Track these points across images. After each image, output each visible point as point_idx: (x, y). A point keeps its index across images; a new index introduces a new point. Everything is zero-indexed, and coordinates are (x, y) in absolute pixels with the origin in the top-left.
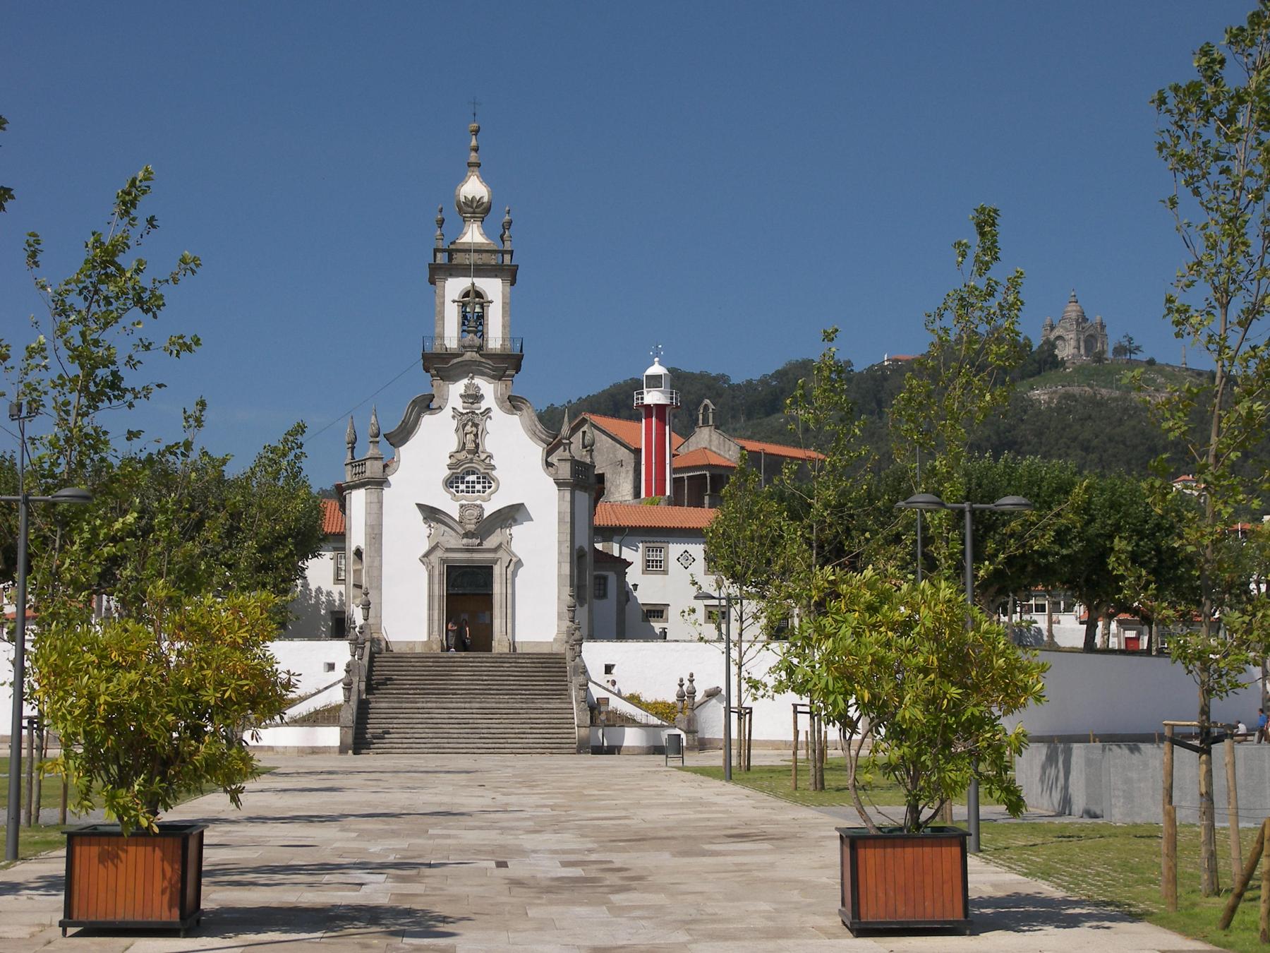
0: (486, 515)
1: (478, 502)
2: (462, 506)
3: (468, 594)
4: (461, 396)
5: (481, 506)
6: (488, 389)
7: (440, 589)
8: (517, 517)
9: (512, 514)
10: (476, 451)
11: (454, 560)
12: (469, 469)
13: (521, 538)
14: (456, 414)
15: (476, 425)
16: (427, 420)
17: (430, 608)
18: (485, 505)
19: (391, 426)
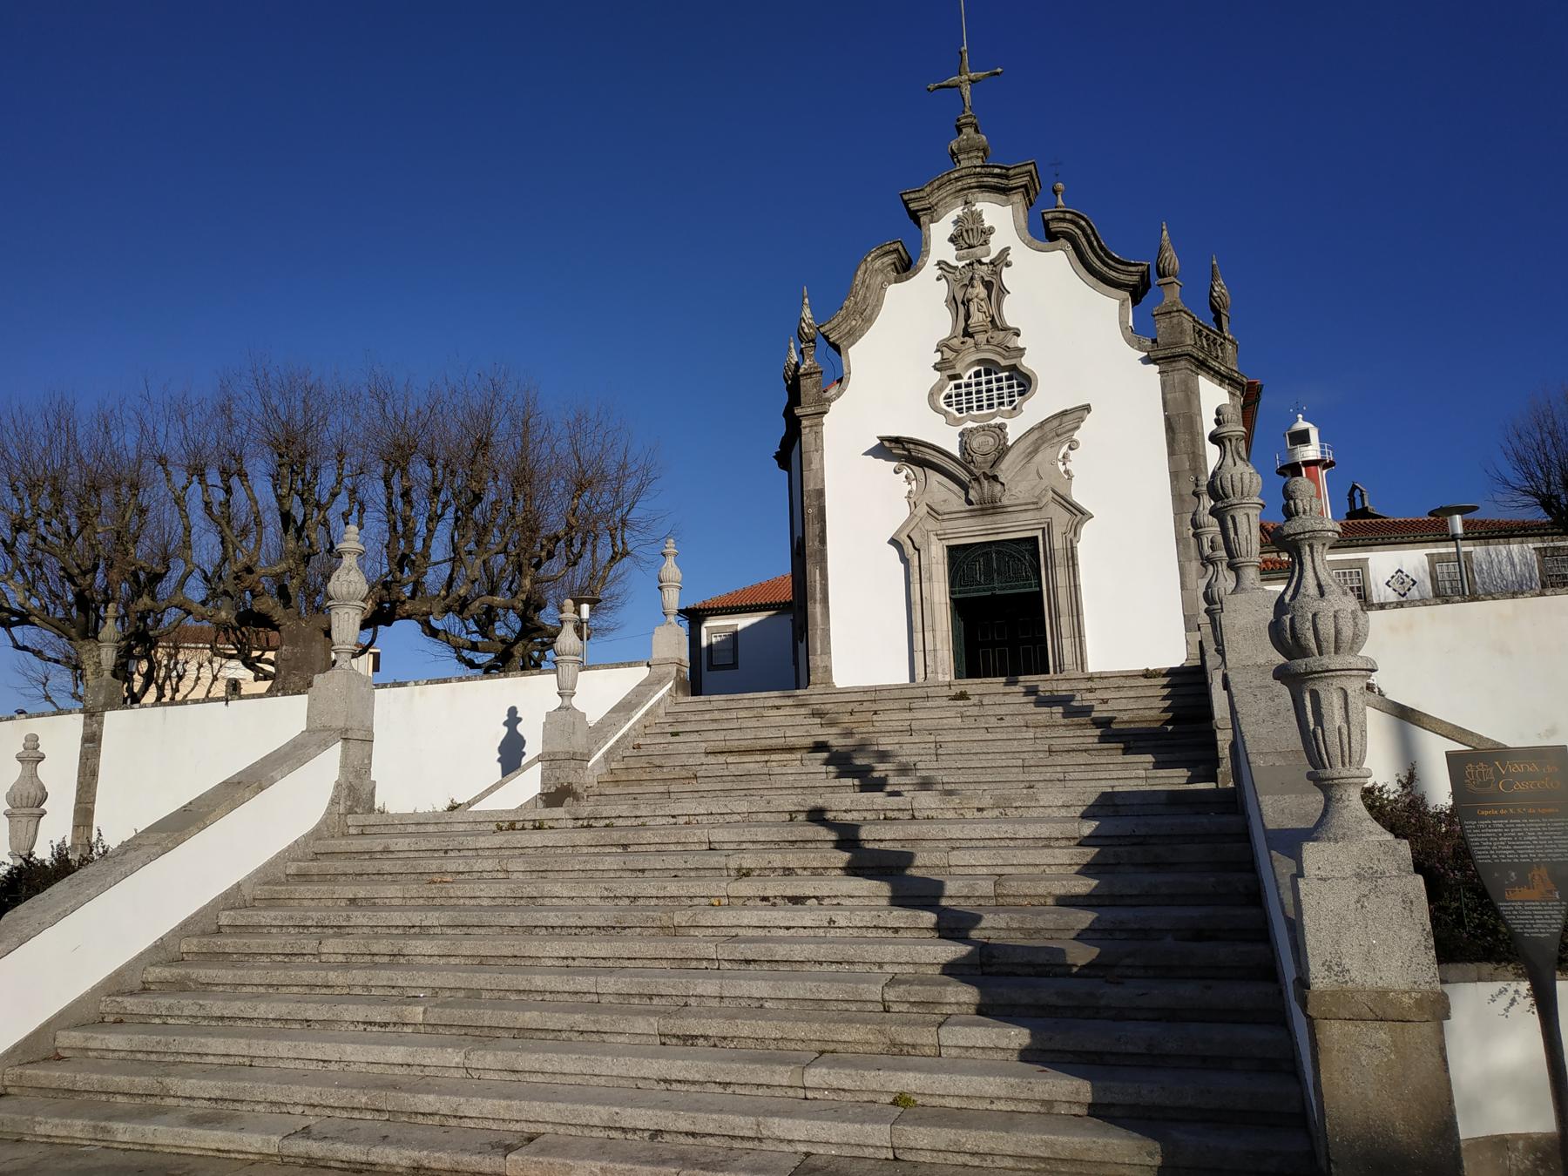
1: (998, 420)
4: (952, 240)
6: (1001, 218)
9: (1064, 424)
12: (986, 362)
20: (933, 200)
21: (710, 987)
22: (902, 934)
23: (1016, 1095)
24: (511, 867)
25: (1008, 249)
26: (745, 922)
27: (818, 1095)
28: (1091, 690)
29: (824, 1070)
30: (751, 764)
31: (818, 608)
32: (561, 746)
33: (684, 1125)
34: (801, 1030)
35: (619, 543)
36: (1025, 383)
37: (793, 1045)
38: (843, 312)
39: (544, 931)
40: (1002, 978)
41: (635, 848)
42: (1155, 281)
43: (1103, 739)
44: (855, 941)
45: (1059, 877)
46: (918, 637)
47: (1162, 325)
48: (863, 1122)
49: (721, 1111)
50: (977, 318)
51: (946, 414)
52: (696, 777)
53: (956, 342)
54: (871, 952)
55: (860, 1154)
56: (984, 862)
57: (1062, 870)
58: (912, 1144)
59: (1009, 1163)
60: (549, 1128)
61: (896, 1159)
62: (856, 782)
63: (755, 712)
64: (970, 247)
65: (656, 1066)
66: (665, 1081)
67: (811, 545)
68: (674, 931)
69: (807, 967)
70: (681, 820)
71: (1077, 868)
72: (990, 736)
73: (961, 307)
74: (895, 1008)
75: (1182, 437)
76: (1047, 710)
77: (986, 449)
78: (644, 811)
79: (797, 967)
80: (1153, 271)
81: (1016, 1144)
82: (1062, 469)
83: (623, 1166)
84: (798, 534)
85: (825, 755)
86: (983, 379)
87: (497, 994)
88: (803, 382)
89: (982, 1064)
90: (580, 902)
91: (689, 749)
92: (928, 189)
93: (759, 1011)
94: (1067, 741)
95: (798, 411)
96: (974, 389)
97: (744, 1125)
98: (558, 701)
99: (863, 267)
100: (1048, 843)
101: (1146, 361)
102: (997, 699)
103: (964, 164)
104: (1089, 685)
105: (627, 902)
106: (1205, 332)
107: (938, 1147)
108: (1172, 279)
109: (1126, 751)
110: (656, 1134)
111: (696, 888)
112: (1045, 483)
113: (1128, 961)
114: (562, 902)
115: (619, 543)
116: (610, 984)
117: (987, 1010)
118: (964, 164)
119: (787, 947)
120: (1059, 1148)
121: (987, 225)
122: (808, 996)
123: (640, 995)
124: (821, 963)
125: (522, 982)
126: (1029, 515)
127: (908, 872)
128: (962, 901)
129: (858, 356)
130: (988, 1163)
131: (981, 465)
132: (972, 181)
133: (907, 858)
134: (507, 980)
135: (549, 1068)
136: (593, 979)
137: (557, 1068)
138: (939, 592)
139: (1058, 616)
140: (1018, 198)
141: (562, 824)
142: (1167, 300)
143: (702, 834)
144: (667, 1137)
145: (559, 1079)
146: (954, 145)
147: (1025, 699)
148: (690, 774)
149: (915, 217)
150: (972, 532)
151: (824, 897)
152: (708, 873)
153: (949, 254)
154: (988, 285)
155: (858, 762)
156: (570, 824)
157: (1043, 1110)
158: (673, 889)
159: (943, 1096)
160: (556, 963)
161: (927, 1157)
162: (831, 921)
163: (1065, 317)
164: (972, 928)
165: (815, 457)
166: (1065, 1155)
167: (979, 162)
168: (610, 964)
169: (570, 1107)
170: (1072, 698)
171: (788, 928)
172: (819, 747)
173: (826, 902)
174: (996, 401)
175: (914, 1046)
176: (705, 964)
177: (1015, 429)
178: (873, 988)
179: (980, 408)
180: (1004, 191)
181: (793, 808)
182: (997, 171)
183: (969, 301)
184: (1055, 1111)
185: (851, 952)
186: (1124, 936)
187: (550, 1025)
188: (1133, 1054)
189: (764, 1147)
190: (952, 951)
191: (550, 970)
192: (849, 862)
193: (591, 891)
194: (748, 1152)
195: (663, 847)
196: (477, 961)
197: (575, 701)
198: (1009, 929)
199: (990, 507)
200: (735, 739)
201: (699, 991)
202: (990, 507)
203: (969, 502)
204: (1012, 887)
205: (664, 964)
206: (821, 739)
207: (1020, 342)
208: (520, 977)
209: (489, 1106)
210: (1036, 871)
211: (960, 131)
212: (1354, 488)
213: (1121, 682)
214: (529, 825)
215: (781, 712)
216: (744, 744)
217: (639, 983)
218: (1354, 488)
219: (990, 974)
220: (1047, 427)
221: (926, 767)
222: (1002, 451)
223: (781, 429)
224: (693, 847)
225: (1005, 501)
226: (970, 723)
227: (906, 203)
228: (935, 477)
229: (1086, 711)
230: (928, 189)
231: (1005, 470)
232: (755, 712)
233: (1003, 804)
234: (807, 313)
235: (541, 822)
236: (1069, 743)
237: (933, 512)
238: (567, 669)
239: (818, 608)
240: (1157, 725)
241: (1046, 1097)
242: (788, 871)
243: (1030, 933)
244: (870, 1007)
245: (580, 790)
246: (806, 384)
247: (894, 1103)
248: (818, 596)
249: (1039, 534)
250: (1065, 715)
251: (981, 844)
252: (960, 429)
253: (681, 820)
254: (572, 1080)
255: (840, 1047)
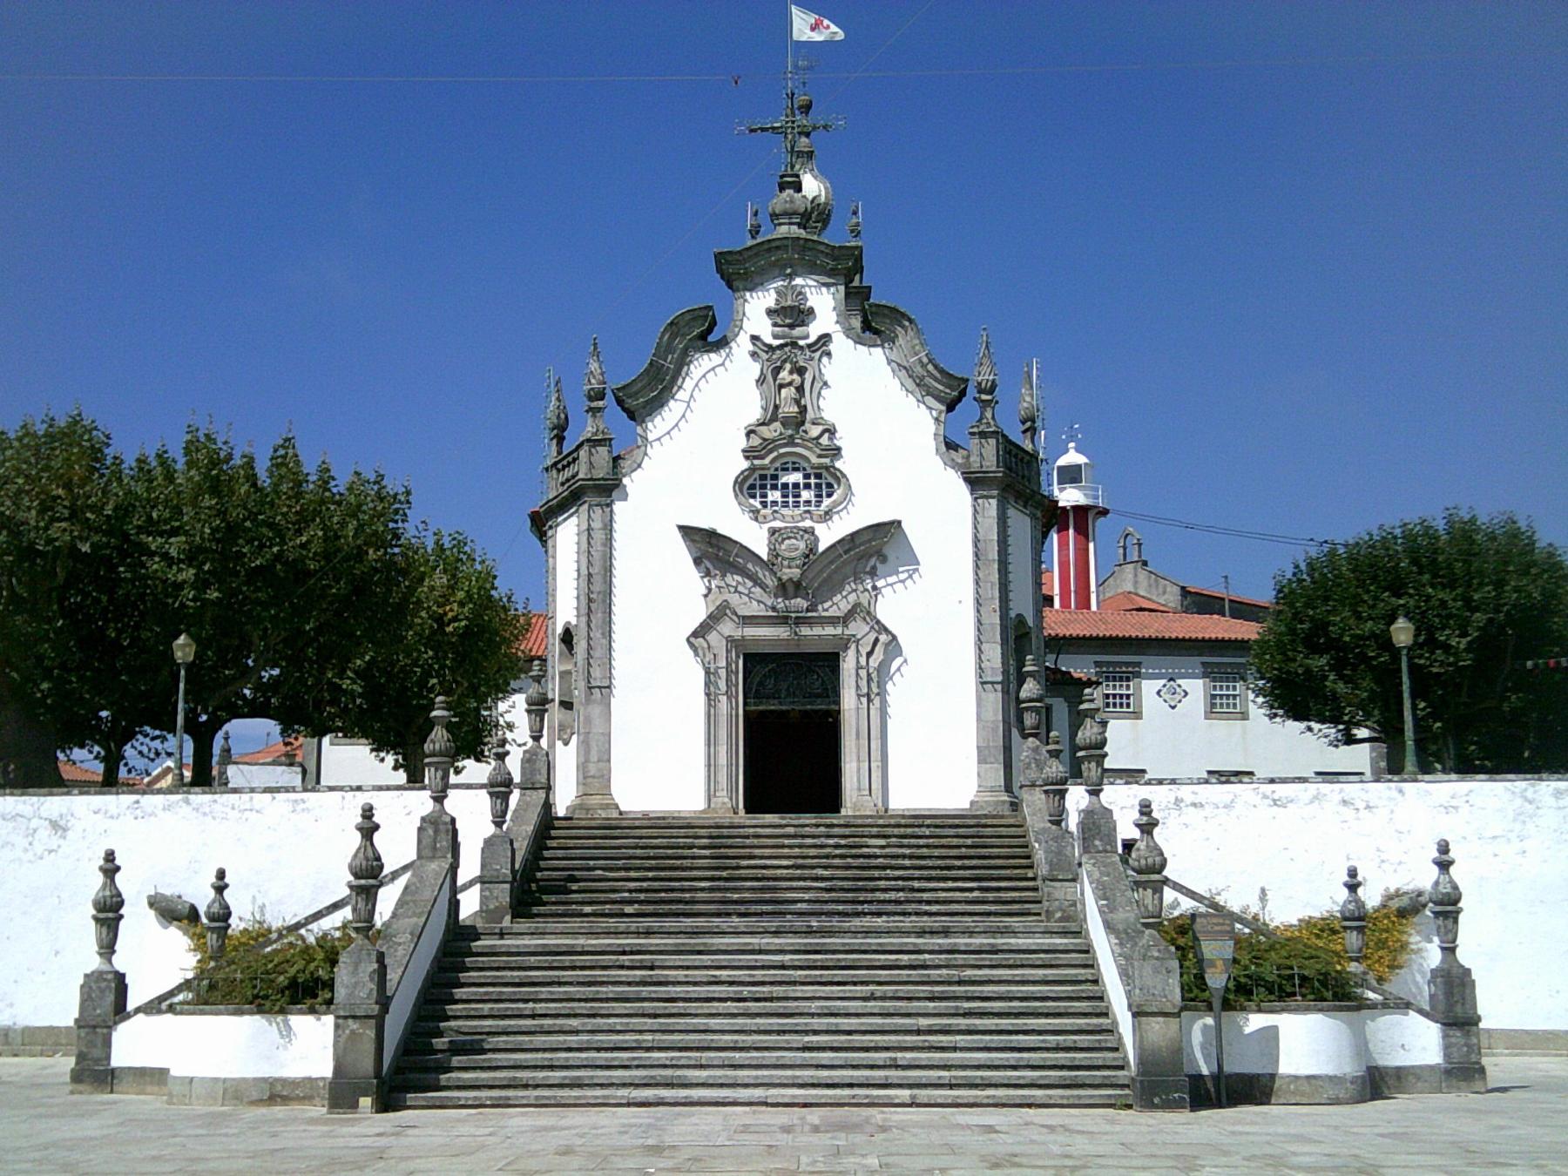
0: (821, 548)
1: (808, 523)
2: (773, 532)
3: (790, 727)
4: (770, 312)
5: (810, 531)
7: (732, 708)
8: (886, 551)
9: (878, 547)
10: (798, 421)
11: (756, 641)
12: (793, 454)
13: (895, 603)
14: (759, 347)
15: (801, 371)
16: (703, 363)
17: (711, 741)
18: (820, 529)
19: (629, 370)
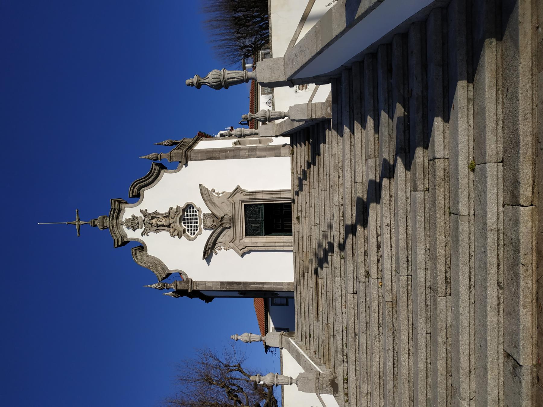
1: (202, 216)
4: (134, 230)
6: (129, 212)
9: (205, 193)
12: (181, 220)
20: (119, 236)
21: (421, 274)
22: (392, 194)
23: (466, 113)
24: (365, 391)
25: (141, 210)
26: (389, 266)
27: (472, 208)
28: (297, 172)
29: (460, 205)
30: (322, 300)
31: (265, 286)
32: (313, 384)
33: (494, 270)
34: (440, 224)
35: (234, 368)
36: (189, 206)
37: (448, 228)
38: (155, 271)
39: (396, 369)
40: (411, 140)
41: (356, 330)
42: (159, 161)
43: (314, 164)
44: (396, 214)
45: (367, 136)
46: (278, 248)
47: (174, 159)
48: (486, 177)
49: (485, 252)
50: (164, 222)
51: (197, 235)
52: (328, 324)
53: (172, 230)
54: (401, 202)
55: (501, 179)
56: (360, 167)
57: (364, 136)
58: (495, 152)
59: (500, 107)
60: (501, 347)
61: (502, 162)
62: (330, 254)
63: (302, 301)
64: (138, 223)
65: (463, 292)
66: (470, 288)
67: (241, 288)
68: (395, 302)
69: (409, 232)
70: (344, 310)
71: (363, 130)
72: (313, 205)
73: (159, 228)
74: (427, 186)
75: (214, 155)
76: (304, 186)
77: (212, 221)
78: (340, 328)
79: (409, 237)
80: (155, 162)
81: (491, 103)
82: (221, 195)
83: (521, 296)
84: (236, 294)
85: (319, 269)
86: (186, 221)
87: (429, 389)
88: (179, 288)
89: (452, 138)
90: (381, 353)
91: (316, 329)
92: (115, 238)
93: (431, 249)
94: (315, 177)
95: (190, 291)
96: (190, 225)
97: (492, 238)
98: (294, 385)
99: (139, 263)
100: (352, 146)
101: (186, 165)
102: (299, 205)
103: (108, 224)
104: (295, 173)
105: (381, 329)
106: (179, 147)
107: (495, 140)
108: (159, 156)
109: (319, 155)
110: (500, 286)
111: (374, 294)
112: (226, 201)
113: (402, 91)
114: (382, 362)
115: (234, 368)
116: (422, 327)
117: (426, 142)
118: (108, 224)
119: (400, 241)
120: (491, 84)
121: (131, 217)
122: (423, 226)
123: (426, 311)
124: (407, 226)
125: (422, 375)
126: (236, 207)
127: (365, 200)
128: (378, 172)
129: (172, 267)
130: (501, 117)
131: (217, 222)
132: (114, 222)
133: (359, 200)
134: (421, 383)
135: (467, 351)
136: (419, 335)
137: (467, 347)
138: (262, 240)
139: (273, 198)
140: (123, 206)
141: (345, 368)
142: (166, 158)
143: (350, 297)
144: (501, 280)
145: (472, 346)
146: (100, 228)
147: (300, 195)
148: (326, 326)
149: (124, 243)
150: (241, 227)
151: (377, 233)
152: (367, 292)
153: (139, 231)
154: (153, 218)
155: (322, 256)
156: (345, 364)
157: (472, 103)
158: (375, 305)
159: (469, 148)
160: (411, 359)
161: (501, 146)
162: (388, 225)
163: (167, 193)
164: (389, 163)
165: (208, 285)
166: (494, 80)
167: (108, 219)
168: (411, 331)
169: (489, 333)
170: (300, 178)
171: (391, 246)
172: (316, 272)
173: (379, 233)
174: (195, 217)
175: (445, 170)
176: (409, 282)
177: (205, 210)
178: (418, 195)
179: (197, 223)
180: (120, 210)
181: (339, 258)
182: (112, 213)
183: (157, 225)
184: (472, 97)
185: (401, 212)
186: (391, 100)
187: (444, 355)
188: (443, 73)
189: (502, 228)
190: (400, 167)
191: (416, 363)
192: (361, 225)
193: (376, 347)
194: (505, 235)
195: (356, 316)
196: (412, 403)
197: (295, 377)
198: (389, 147)
199: (233, 220)
200: (313, 309)
201: (423, 280)
202: (233, 220)
203: (230, 227)
204: (371, 151)
205: (410, 303)
206: (313, 272)
207: (175, 207)
208: (420, 376)
209: (491, 382)
210: (364, 146)
211: (96, 226)
212: (241, 123)
213: (295, 162)
214: (346, 386)
215: (302, 290)
216: (315, 304)
217: (421, 311)
218: (241, 123)
219: (409, 149)
220: (206, 199)
221: (324, 227)
222: (213, 215)
223: (197, 300)
224: (356, 301)
225: (231, 215)
226: (308, 214)
227: (118, 246)
228: (220, 239)
229: (304, 172)
230: (115, 238)
231: (219, 214)
232: (302, 301)
233: (337, 168)
234: (154, 286)
235: (345, 379)
236: (316, 176)
237: (233, 241)
238: (281, 380)
239: (265, 286)
240: (310, 146)
241: (466, 100)
242: (366, 254)
243: (390, 139)
244: (427, 197)
245: (332, 376)
246: (180, 287)
247: (473, 171)
248: (261, 286)
249: (243, 204)
250: (306, 180)
251: (353, 173)
252: (203, 230)
253: (344, 310)
254: (472, 339)
255: (447, 205)
